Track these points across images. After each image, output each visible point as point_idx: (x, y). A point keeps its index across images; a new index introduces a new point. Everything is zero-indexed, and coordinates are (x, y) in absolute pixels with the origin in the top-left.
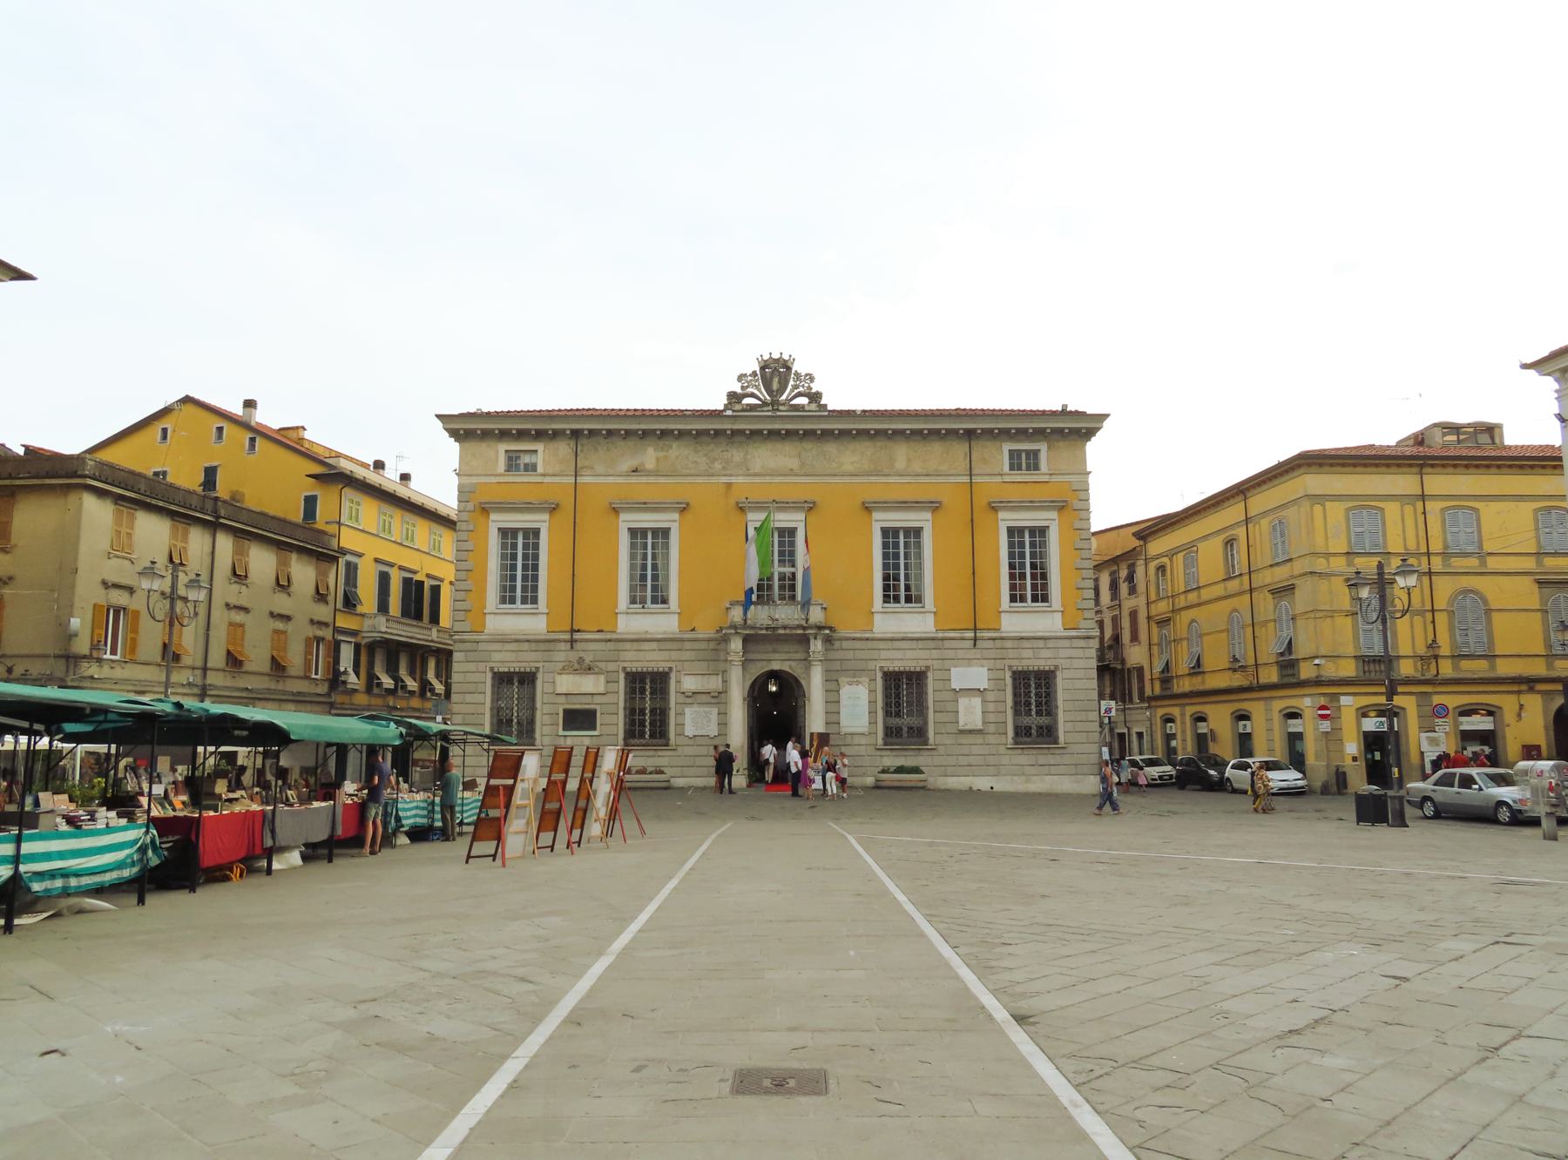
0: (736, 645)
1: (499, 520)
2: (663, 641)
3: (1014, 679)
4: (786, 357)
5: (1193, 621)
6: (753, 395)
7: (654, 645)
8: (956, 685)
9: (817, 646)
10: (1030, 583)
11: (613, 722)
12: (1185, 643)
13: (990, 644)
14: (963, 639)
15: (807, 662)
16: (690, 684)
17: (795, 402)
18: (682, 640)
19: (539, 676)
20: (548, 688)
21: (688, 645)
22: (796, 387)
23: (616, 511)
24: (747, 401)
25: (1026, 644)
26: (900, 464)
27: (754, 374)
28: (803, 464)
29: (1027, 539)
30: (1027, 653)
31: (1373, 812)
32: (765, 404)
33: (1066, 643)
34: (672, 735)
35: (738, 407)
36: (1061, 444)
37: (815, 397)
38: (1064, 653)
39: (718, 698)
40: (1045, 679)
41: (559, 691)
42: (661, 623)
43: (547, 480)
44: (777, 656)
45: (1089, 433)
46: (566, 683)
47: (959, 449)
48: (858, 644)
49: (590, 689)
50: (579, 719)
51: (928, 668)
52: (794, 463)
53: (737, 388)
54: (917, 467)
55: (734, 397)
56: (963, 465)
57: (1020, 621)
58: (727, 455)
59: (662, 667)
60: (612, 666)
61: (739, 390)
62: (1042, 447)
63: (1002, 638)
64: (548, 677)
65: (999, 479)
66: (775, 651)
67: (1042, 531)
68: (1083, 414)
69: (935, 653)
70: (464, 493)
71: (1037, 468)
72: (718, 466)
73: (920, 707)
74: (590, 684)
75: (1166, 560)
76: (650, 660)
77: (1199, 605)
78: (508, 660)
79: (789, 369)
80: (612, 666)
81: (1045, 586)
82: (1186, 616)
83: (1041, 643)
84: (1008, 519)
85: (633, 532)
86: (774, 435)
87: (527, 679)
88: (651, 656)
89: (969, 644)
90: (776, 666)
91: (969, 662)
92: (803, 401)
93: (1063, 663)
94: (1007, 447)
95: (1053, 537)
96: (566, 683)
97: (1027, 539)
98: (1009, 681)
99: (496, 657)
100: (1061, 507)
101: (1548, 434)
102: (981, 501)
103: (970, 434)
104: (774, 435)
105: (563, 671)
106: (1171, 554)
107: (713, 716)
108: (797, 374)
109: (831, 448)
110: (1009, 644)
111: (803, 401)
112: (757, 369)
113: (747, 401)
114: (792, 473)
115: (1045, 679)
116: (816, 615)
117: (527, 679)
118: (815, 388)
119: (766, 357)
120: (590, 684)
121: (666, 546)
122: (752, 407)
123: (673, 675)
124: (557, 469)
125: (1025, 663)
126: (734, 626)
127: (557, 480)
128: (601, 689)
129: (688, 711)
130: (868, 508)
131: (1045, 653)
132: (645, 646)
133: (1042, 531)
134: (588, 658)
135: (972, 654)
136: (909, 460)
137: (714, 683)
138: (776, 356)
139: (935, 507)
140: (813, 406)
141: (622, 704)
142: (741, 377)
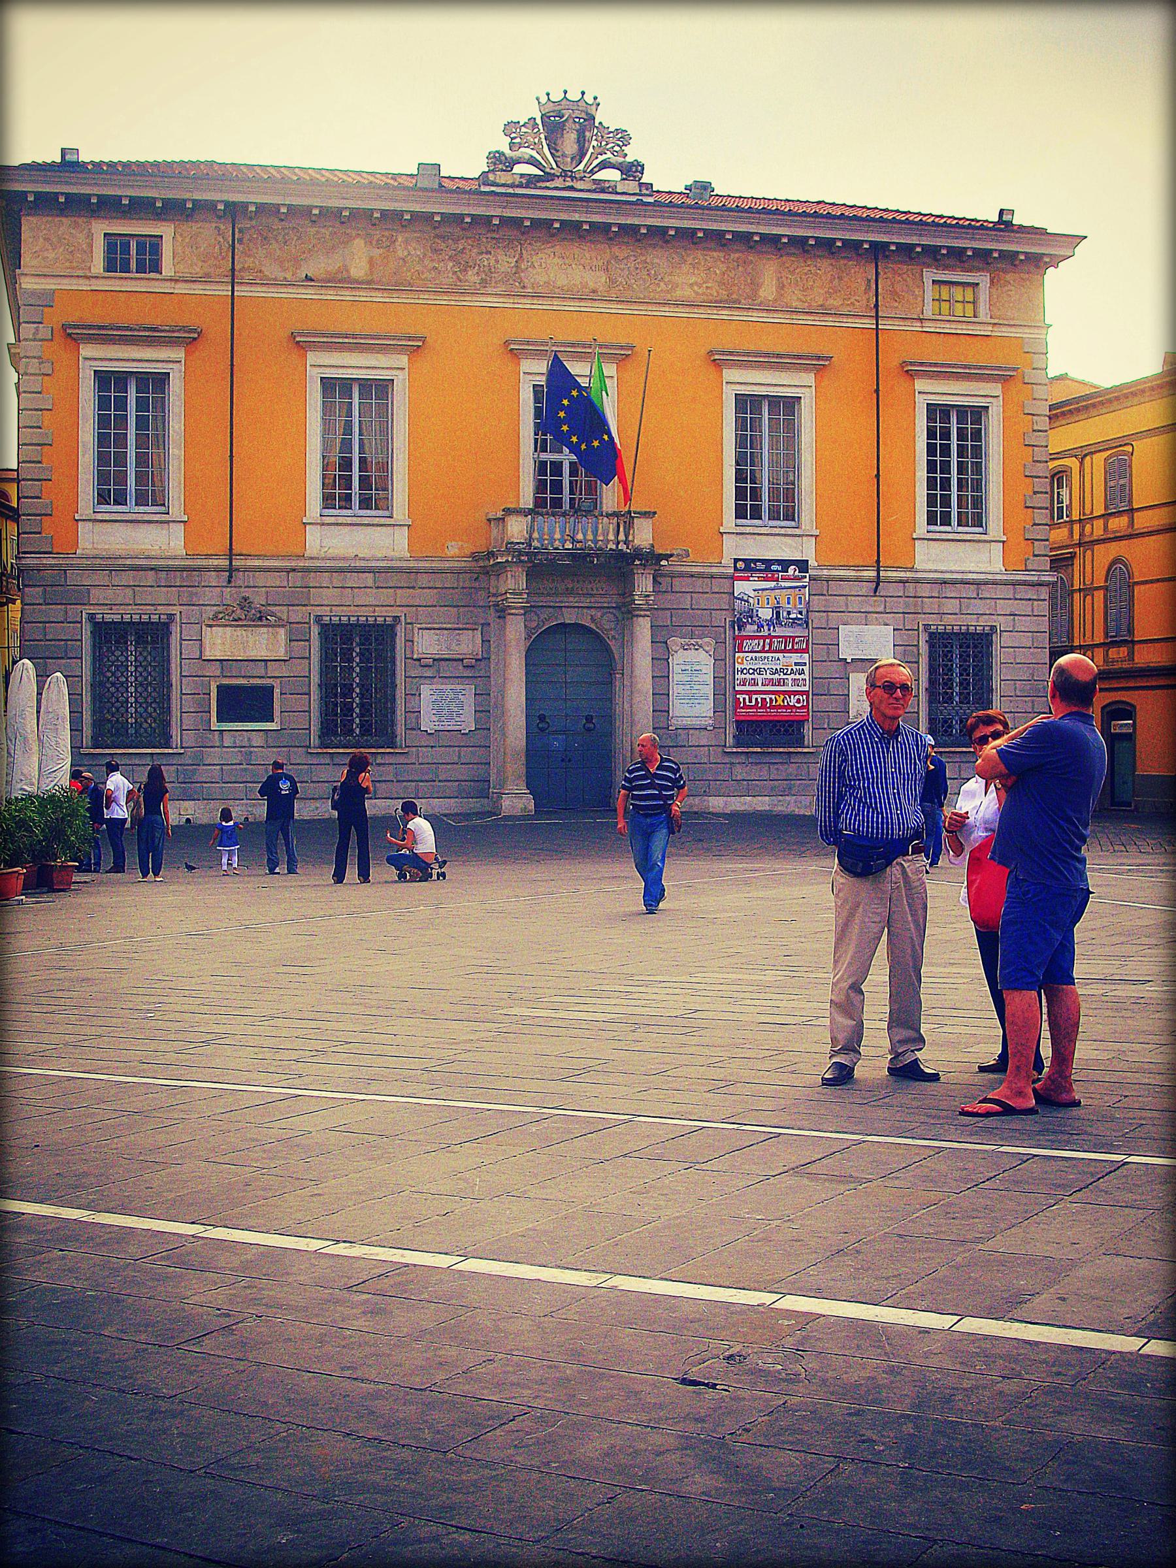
0: (515, 582)
1: (96, 356)
2: (382, 573)
3: (931, 645)
5: (1116, 561)
7: (369, 579)
8: (846, 653)
9: (644, 584)
10: (955, 497)
11: (299, 709)
12: (1099, 595)
13: (897, 590)
14: (859, 580)
15: (626, 611)
16: (428, 644)
17: (600, 175)
18: (417, 572)
19: (175, 629)
20: (191, 650)
21: (424, 580)
23: (718, 365)
24: (519, 169)
25: (950, 592)
26: (768, 291)
28: (612, 281)
29: (132, 394)
30: (951, 606)
31: (355, 840)
32: (549, 177)
33: (1008, 592)
34: (400, 729)
36: (1008, 277)
37: (632, 170)
38: (1004, 607)
39: (477, 670)
40: (976, 646)
41: (208, 655)
42: (380, 541)
43: (181, 288)
44: (573, 601)
45: (1038, 263)
46: (221, 643)
47: (859, 274)
48: (700, 585)
49: (263, 654)
50: (244, 701)
51: (396, 619)
52: (596, 280)
53: (503, 144)
54: (794, 298)
55: (499, 161)
56: (863, 300)
57: (943, 556)
58: (485, 260)
59: (382, 615)
60: (298, 614)
61: (508, 152)
62: (166, 230)
63: (917, 581)
64: (191, 632)
65: (84, 285)
66: (569, 592)
67: (978, 414)
68: (1041, 232)
69: (402, 596)
71: (156, 267)
72: (472, 277)
74: (263, 644)
75: (1073, 463)
76: (367, 604)
77: (1131, 536)
78: (117, 602)
80: (298, 614)
81: (978, 502)
82: (1104, 555)
83: (971, 591)
84: (324, 363)
85: (328, 385)
86: (572, 230)
87: (154, 635)
88: (369, 597)
89: (866, 588)
90: (569, 618)
91: (866, 617)
92: (612, 175)
93: (1001, 623)
94: (100, 228)
95: (176, 386)
96: (221, 643)
97: (132, 394)
98: (924, 648)
99: (108, 595)
100: (1005, 377)
102: (890, 361)
103: (878, 251)
104: (572, 230)
105: (215, 621)
106: (1083, 453)
107: (463, 702)
109: (658, 258)
110: (924, 590)
111: (612, 175)
113: (519, 169)
114: (593, 295)
115: (976, 646)
116: (643, 536)
117: (154, 635)
118: (632, 154)
119: (557, 96)
120: (263, 644)
121: (162, 405)
122: (531, 181)
123: (400, 631)
124: (198, 270)
125: (949, 620)
126: (511, 547)
127: (198, 289)
128: (281, 653)
129: (426, 690)
130: (717, 361)
131: (979, 606)
132: (352, 580)
133: (978, 414)
134: (258, 600)
135: (877, 604)
136: (781, 287)
137: (468, 644)
138: (574, 96)
139: (819, 364)
140: (632, 186)
141: (315, 679)
142: (510, 128)
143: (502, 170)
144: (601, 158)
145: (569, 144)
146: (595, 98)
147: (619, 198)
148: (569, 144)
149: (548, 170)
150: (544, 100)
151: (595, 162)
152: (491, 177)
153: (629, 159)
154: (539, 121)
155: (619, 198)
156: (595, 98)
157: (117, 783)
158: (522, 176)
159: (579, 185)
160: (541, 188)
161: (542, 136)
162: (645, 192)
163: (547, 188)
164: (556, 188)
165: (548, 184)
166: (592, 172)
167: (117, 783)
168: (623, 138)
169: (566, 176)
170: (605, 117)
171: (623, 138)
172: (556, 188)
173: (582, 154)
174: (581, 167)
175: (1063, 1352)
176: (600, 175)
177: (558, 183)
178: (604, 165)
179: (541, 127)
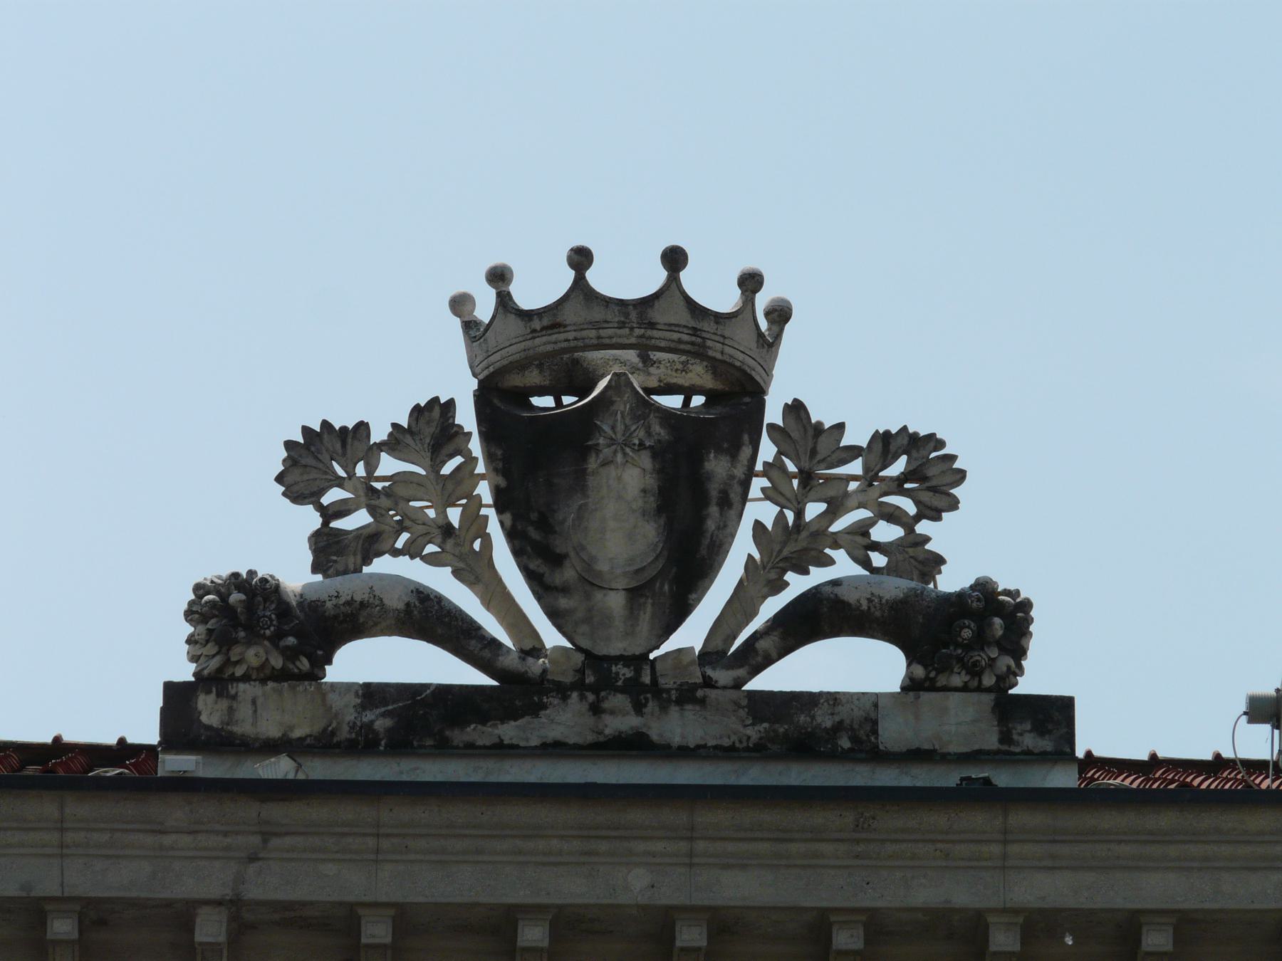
4: (712, 288)
6: (429, 619)
22: (790, 548)
24: (365, 661)
27: (431, 427)
35: (268, 712)
37: (970, 635)
53: (281, 549)
61: (295, 573)
70: (856, 458)
73: (1001, 732)
79: (740, 394)
92: (860, 667)
101: (692, 405)
108: (808, 437)
112: (461, 389)
113: (365, 661)
118: (967, 551)
119: (539, 287)
122: (416, 716)
138: (627, 276)
140: (959, 719)
142: (314, 460)
143: (266, 675)
144: (797, 584)
145: (617, 514)
146: (751, 282)
147: (887, 777)
148: (617, 514)
149: (511, 661)
150: (485, 309)
151: (771, 607)
152: (209, 711)
153: (950, 581)
154: (466, 417)
155: (887, 777)
156: (751, 282)
157: (439, 631)
158: (372, 694)
159: (677, 726)
160: (471, 750)
161: (484, 491)
162: (1029, 741)
163: (502, 750)
164: (555, 749)
165: (508, 731)
166: (756, 657)
167: (439, 631)
168: (924, 470)
169: (606, 684)
170: (826, 376)
171: (924, 470)
172: (555, 749)
173: (687, 568)
174: (691, 634)
175: (614, 316)
176: (780, 677)
177: (565, 720)
178: (813, 620)
179: (475, 446)
